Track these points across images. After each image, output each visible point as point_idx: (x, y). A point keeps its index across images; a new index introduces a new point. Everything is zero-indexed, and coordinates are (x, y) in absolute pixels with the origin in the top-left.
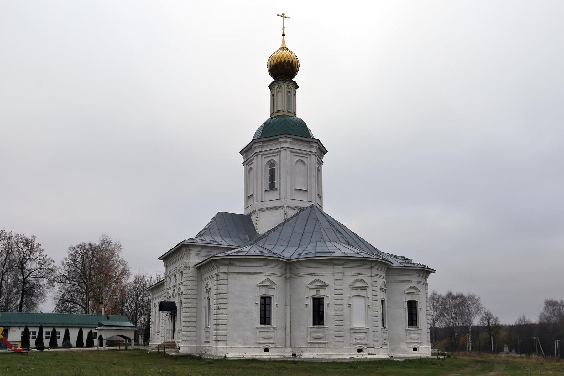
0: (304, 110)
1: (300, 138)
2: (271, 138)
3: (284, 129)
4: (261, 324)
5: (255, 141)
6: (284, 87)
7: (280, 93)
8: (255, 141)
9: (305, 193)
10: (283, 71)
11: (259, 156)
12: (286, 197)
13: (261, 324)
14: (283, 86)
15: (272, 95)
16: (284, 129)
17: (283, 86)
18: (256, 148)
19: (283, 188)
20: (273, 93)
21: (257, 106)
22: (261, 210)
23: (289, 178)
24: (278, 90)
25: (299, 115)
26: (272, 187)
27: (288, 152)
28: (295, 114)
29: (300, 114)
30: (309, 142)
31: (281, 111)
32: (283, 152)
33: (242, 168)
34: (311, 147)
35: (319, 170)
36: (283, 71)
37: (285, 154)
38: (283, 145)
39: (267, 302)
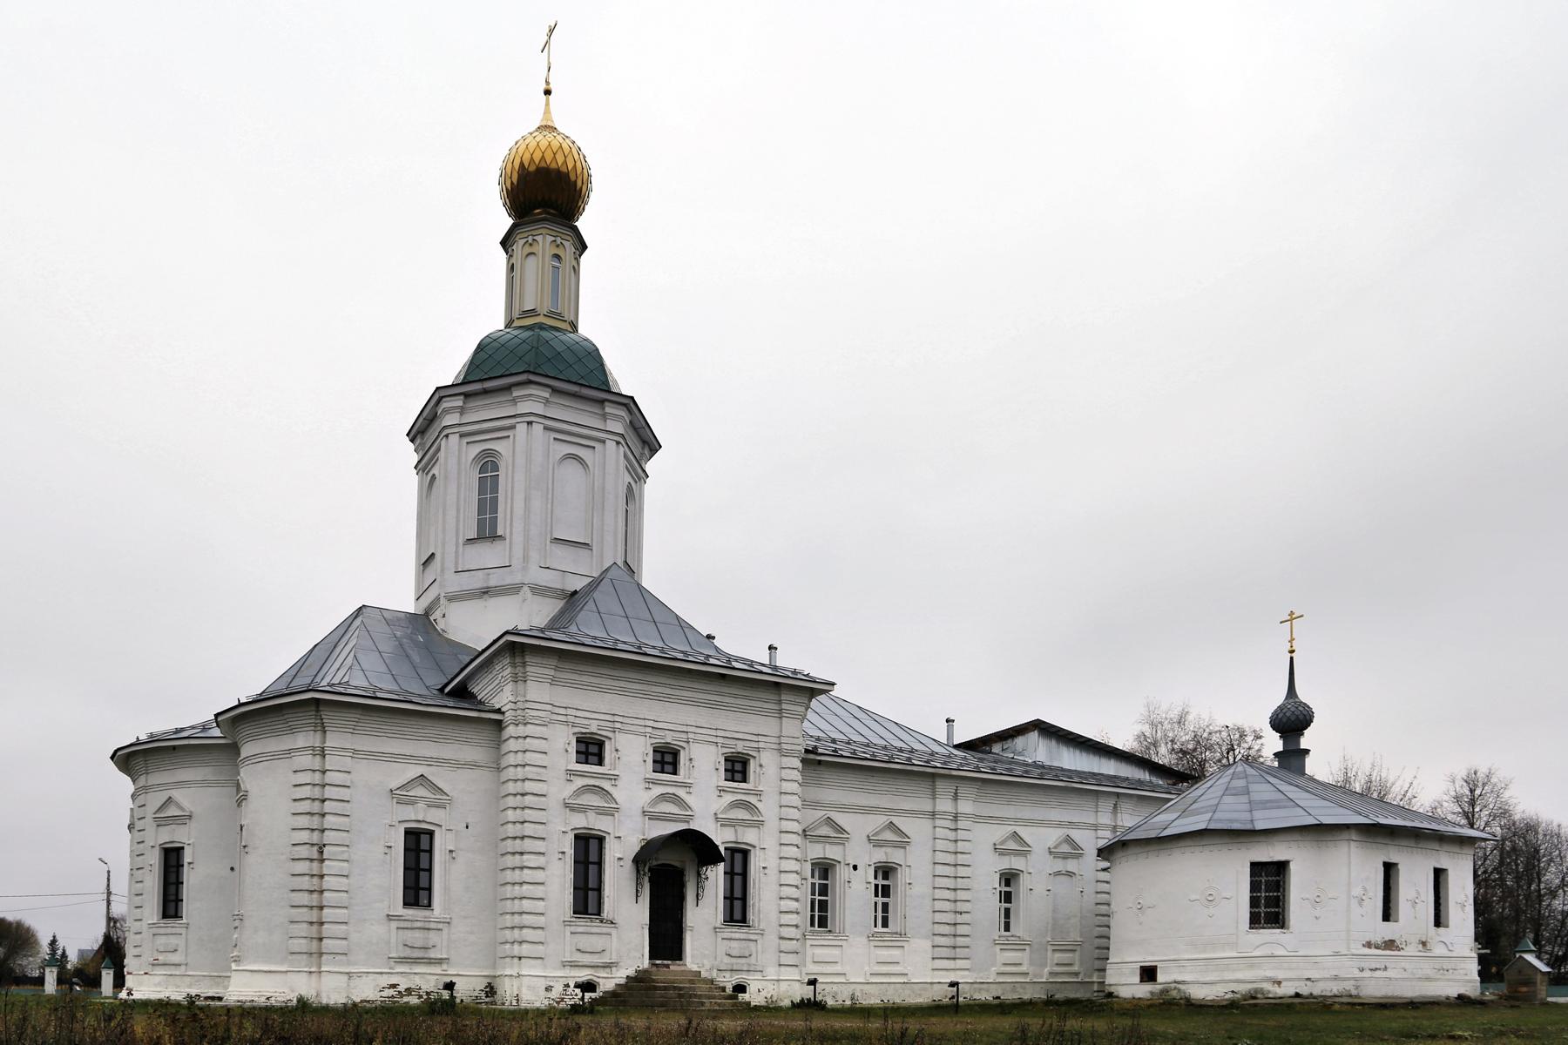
0: (601, 319)
1: (575, 388)
2: (488, 385)
3: (539, 366)
4: (406, 904)
5: (443, 393)
6: (544, 240)
7: (531, 261)
8: (443, 393)
9: (584, 552)
10: (545, 197)
11: (454, 439)
12: (526, 558)
13: (406, 904)
14: (539, 238)
15: (511, 268)
16: (539, 366)
17: (539, 238)
18: (447, 411)
19: (518, 538)
20: (513, 260)
21: (473, 303)
22: (452, 598)
23: (537, 504)
24: (528, 250)
25: (585, 329)
26: (487, 533)
27: (538, 429)
28: (574, 327)
29: (591, 327)
30: (602, 402)
31: (532, 312)
32: (521, 429)
33: (413, 480)
34: (604, 417)
35: (632, 496)
36: (545, 197)
37: (529, 439)
38: (523, 407)
39: (424, 845)
